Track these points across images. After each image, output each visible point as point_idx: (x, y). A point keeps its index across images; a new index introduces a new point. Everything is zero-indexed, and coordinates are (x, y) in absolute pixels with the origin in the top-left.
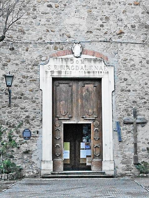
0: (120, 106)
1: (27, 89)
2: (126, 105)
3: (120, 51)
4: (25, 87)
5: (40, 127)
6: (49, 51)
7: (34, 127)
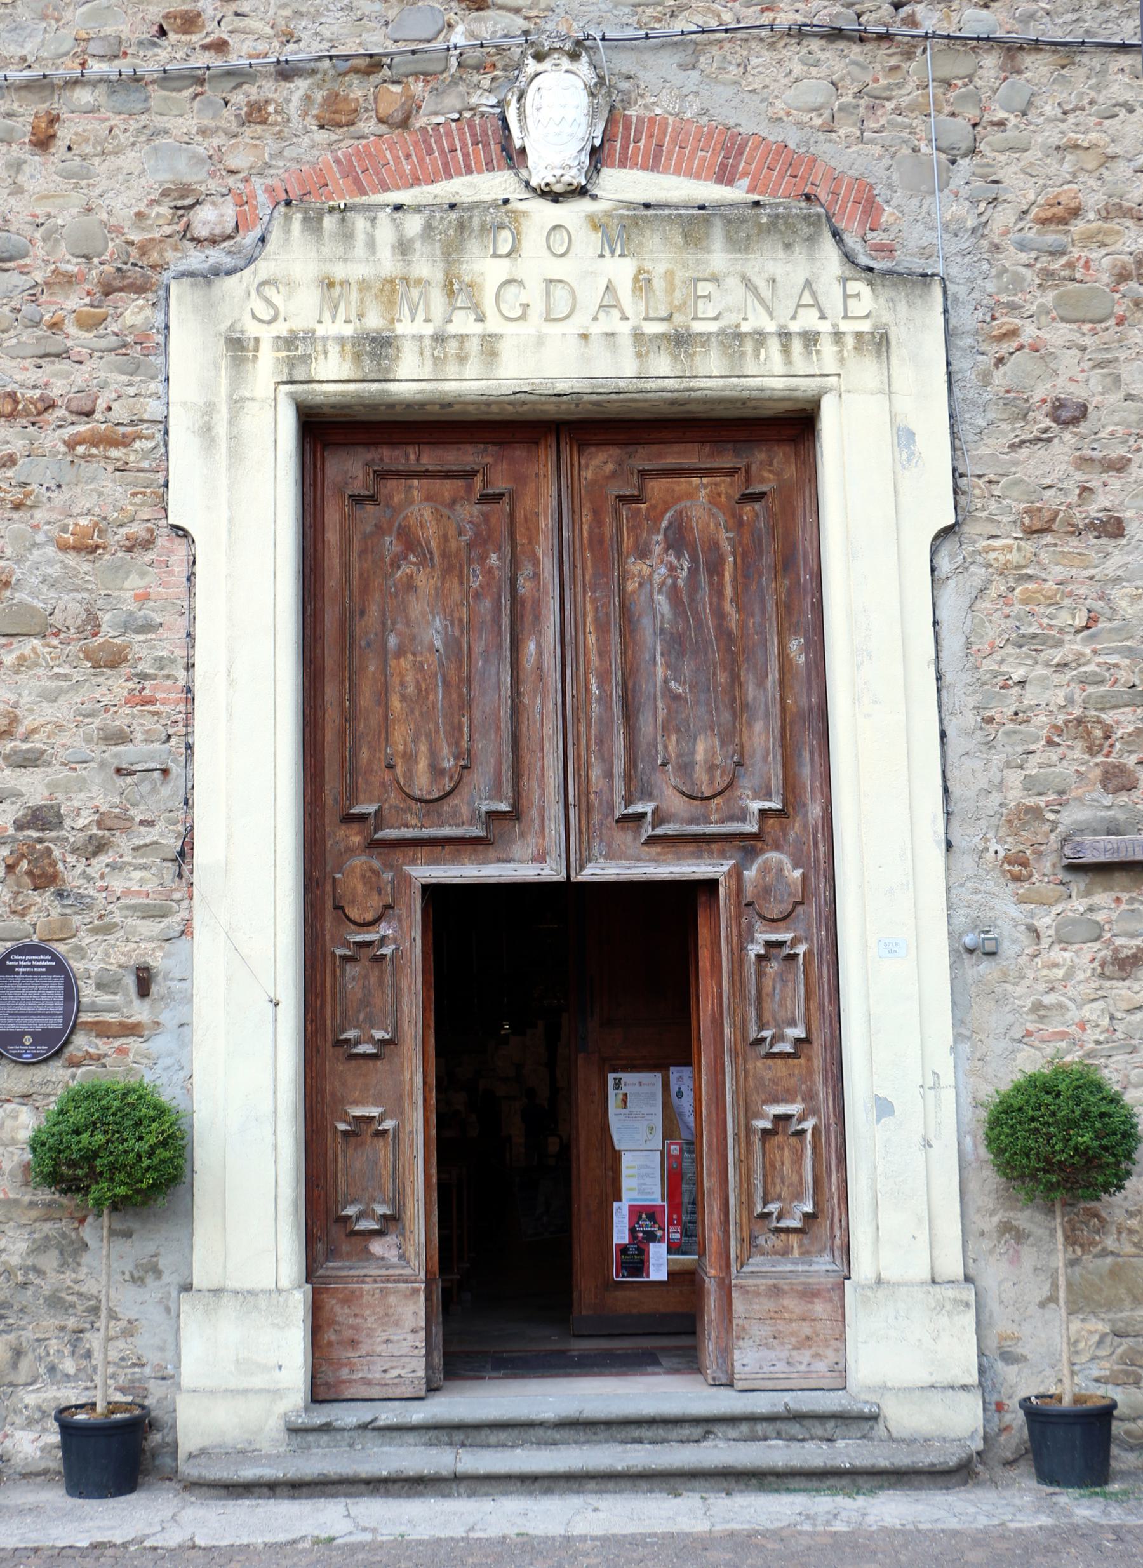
0: (1022, 683)
1: (36, 528)
2: (1084, 681)
3: (1001, 124)
4: (17, 507)
5: (174, 922)
6: (271, 145)
7: (107, 929)
